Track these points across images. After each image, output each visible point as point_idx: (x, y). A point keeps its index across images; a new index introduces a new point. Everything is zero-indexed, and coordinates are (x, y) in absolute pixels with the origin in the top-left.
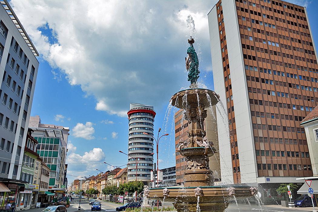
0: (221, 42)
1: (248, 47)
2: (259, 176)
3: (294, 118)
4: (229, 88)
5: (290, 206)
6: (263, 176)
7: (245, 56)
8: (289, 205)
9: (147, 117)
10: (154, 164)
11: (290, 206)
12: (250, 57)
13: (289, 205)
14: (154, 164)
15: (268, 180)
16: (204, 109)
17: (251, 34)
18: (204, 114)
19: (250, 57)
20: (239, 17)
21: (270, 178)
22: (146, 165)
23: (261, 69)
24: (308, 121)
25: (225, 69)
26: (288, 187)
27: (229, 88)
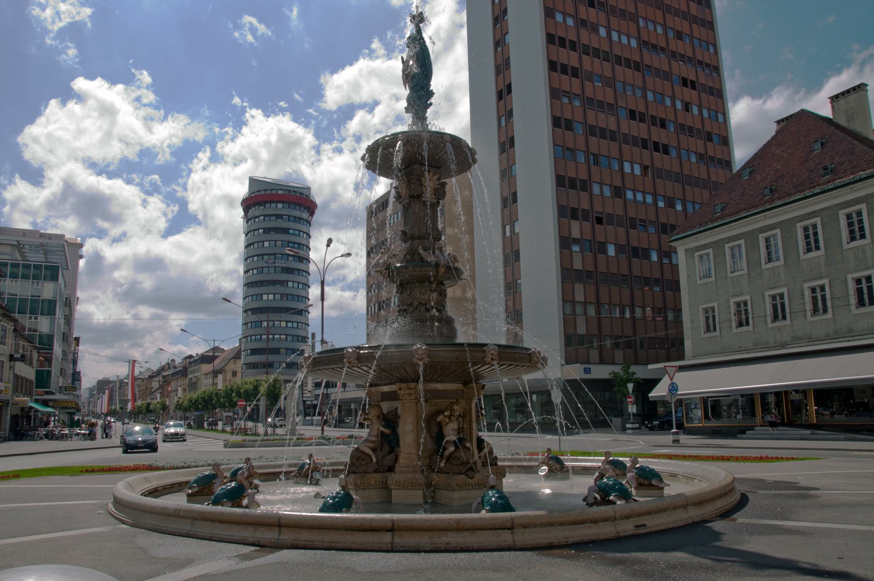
0: (498, 73)
1: (562, 42)
2: (569, 361)
3: (651, 145)
4: (505, 92)
5: (629, 429)
6: (577, 362)
7: (552, 66)
8: (628, 426)
9: (292, 319)
10: (310, 336)
11: (629, 429)
12: (564, 69)
13: (628, 426)
14: (310, 336)
15: (587, 371)
16: (439, 179)
17: (579, 117)
18: (440, 192)
19: (564, 69)
20: (555, 94)
21: (592, 367)
22: (289, 338)
23: (590, 101)
24: (687, 234)
25: (500, 96)
26: (630, 386)
27: (505, 92)
